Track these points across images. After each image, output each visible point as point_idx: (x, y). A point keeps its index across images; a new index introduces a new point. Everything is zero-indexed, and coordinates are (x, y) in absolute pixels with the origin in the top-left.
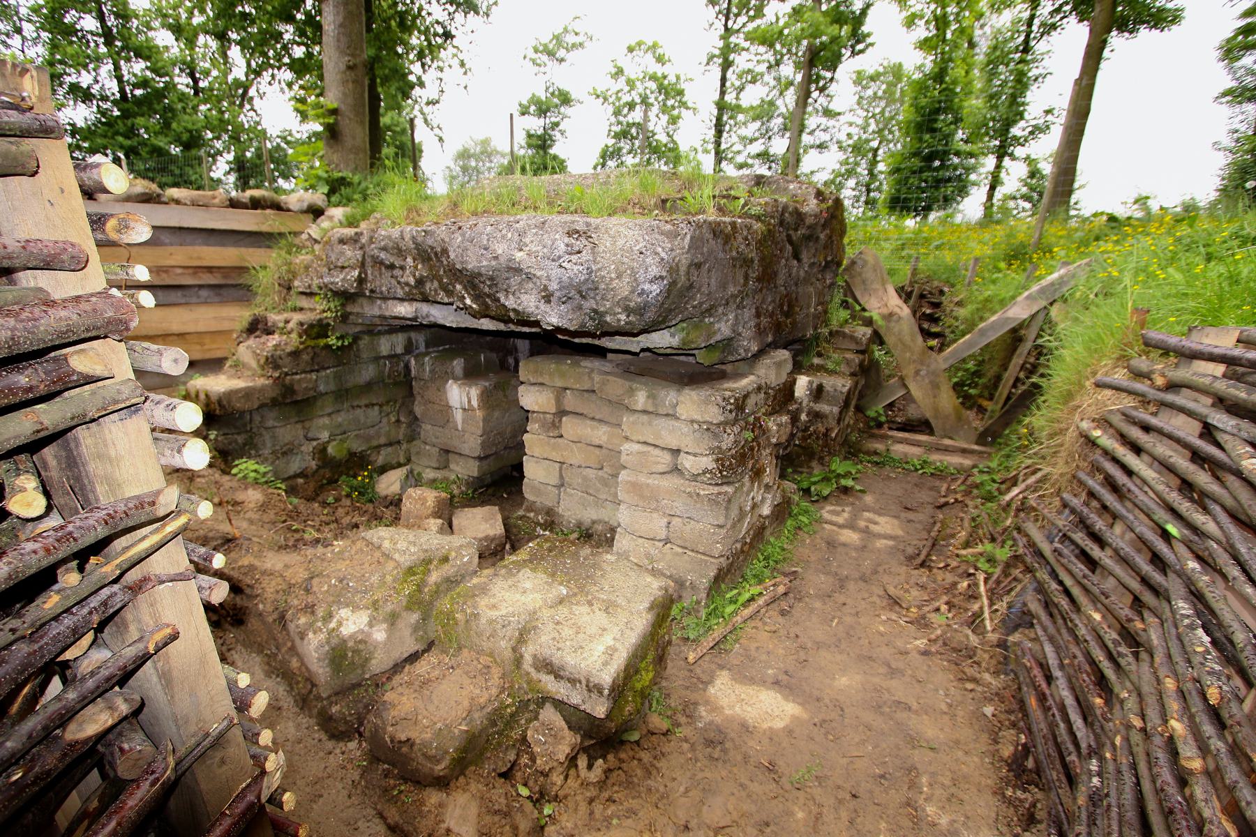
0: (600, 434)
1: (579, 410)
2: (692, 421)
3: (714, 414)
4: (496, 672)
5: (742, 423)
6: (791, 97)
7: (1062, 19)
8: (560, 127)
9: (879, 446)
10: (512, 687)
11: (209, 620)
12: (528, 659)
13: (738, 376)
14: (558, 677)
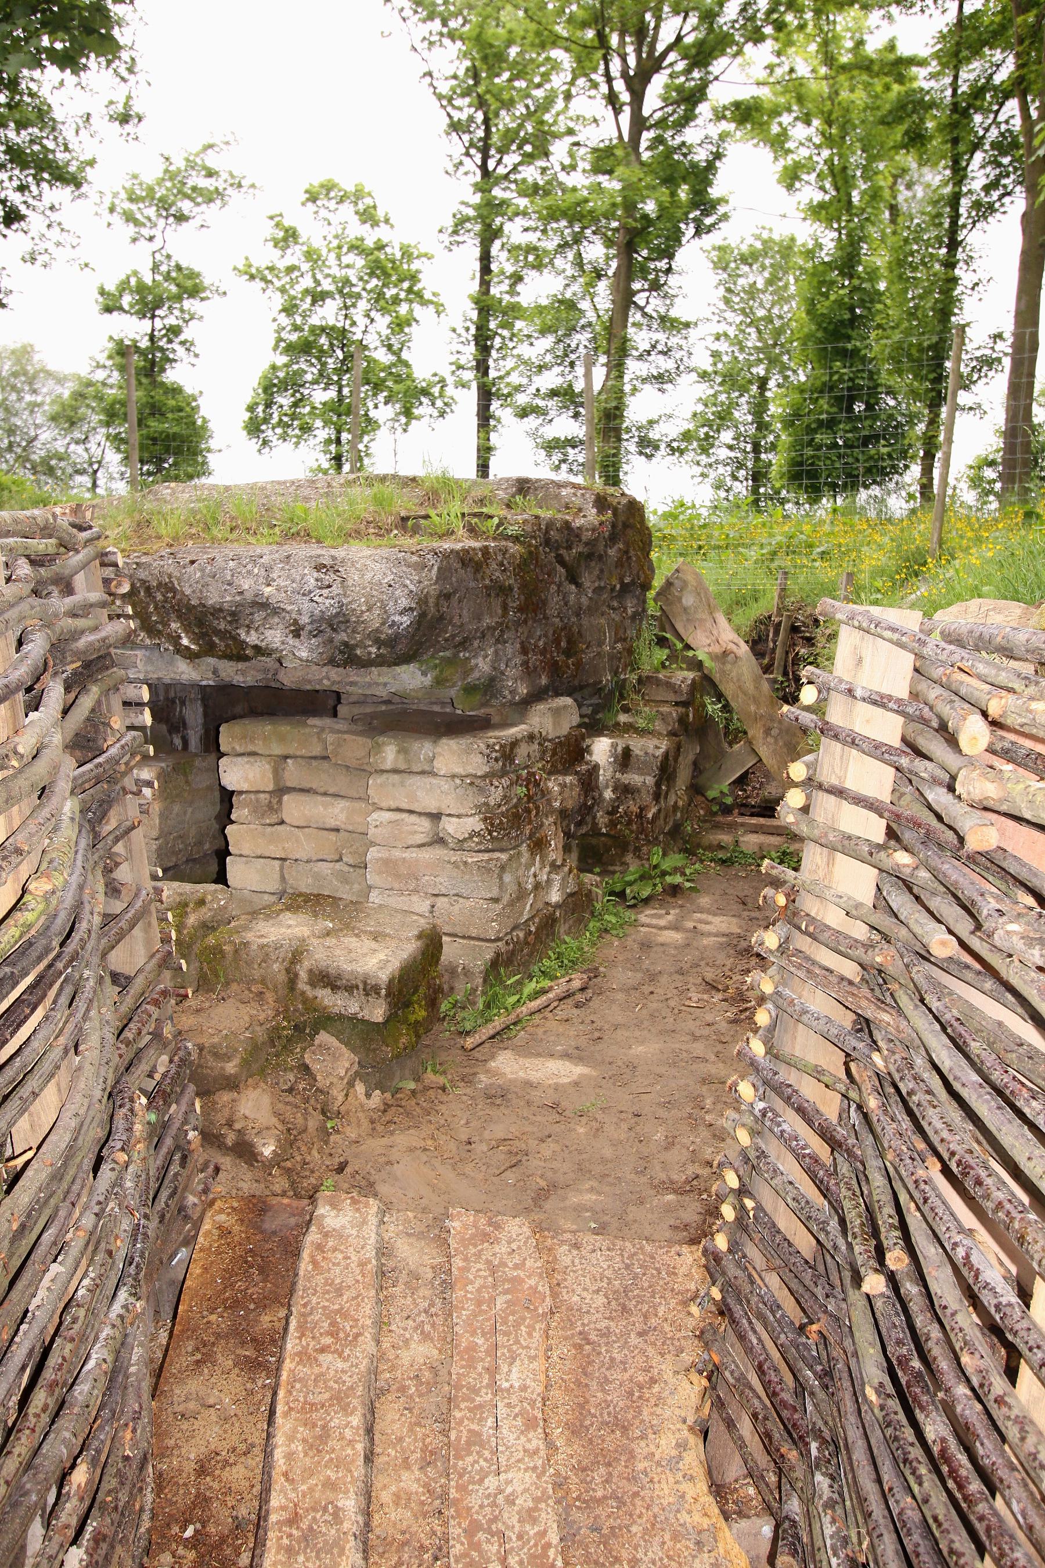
0: (337, 812)
1: (306, 785)
2: (453, 776)
3: (478, 765)
4: (270, 997)
5: (513, 776)
6: (604, 294)
7: (1003, 196)
8: (182, 337)
9: (725, 838)
10: (287, 1010)
12: (303, 975)
13: (505, 725)
14: (335, 988)
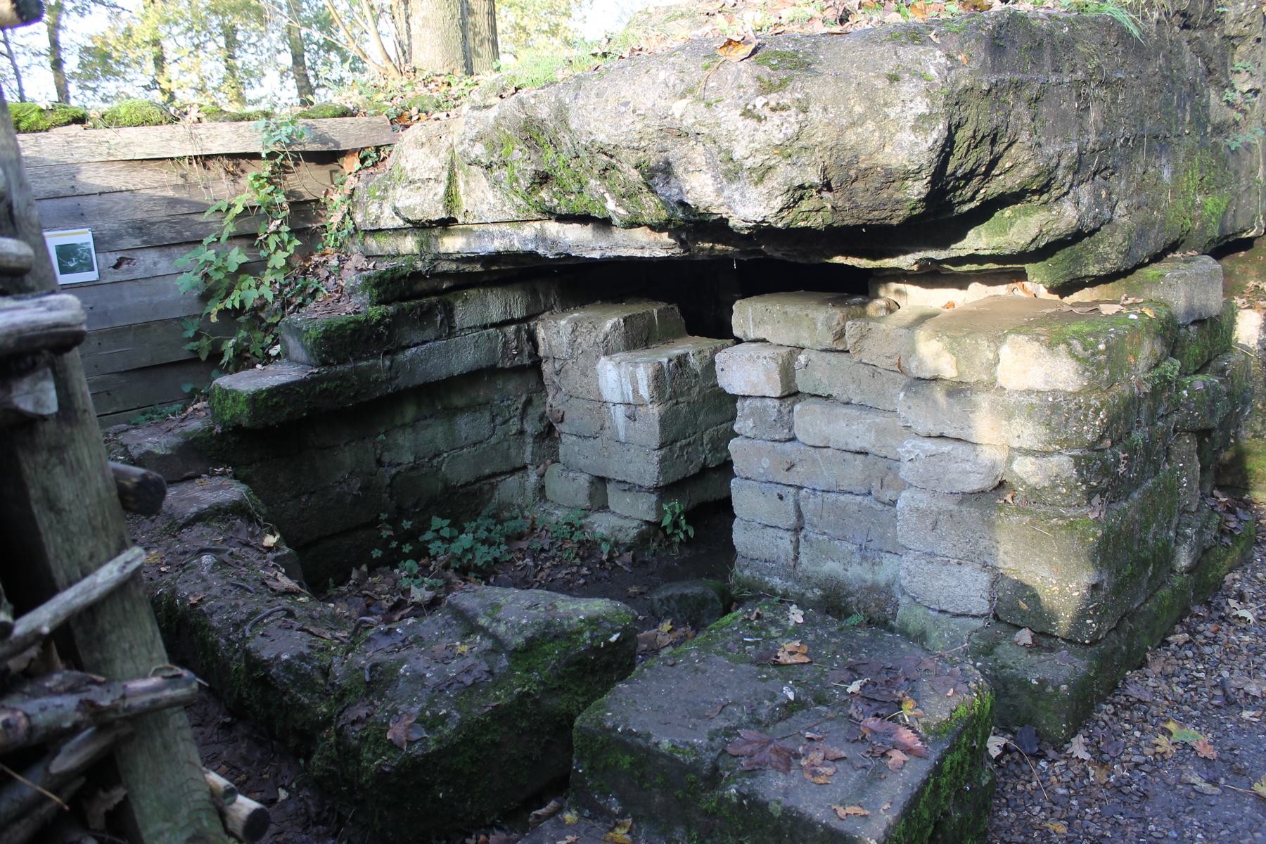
11: (261, 392)
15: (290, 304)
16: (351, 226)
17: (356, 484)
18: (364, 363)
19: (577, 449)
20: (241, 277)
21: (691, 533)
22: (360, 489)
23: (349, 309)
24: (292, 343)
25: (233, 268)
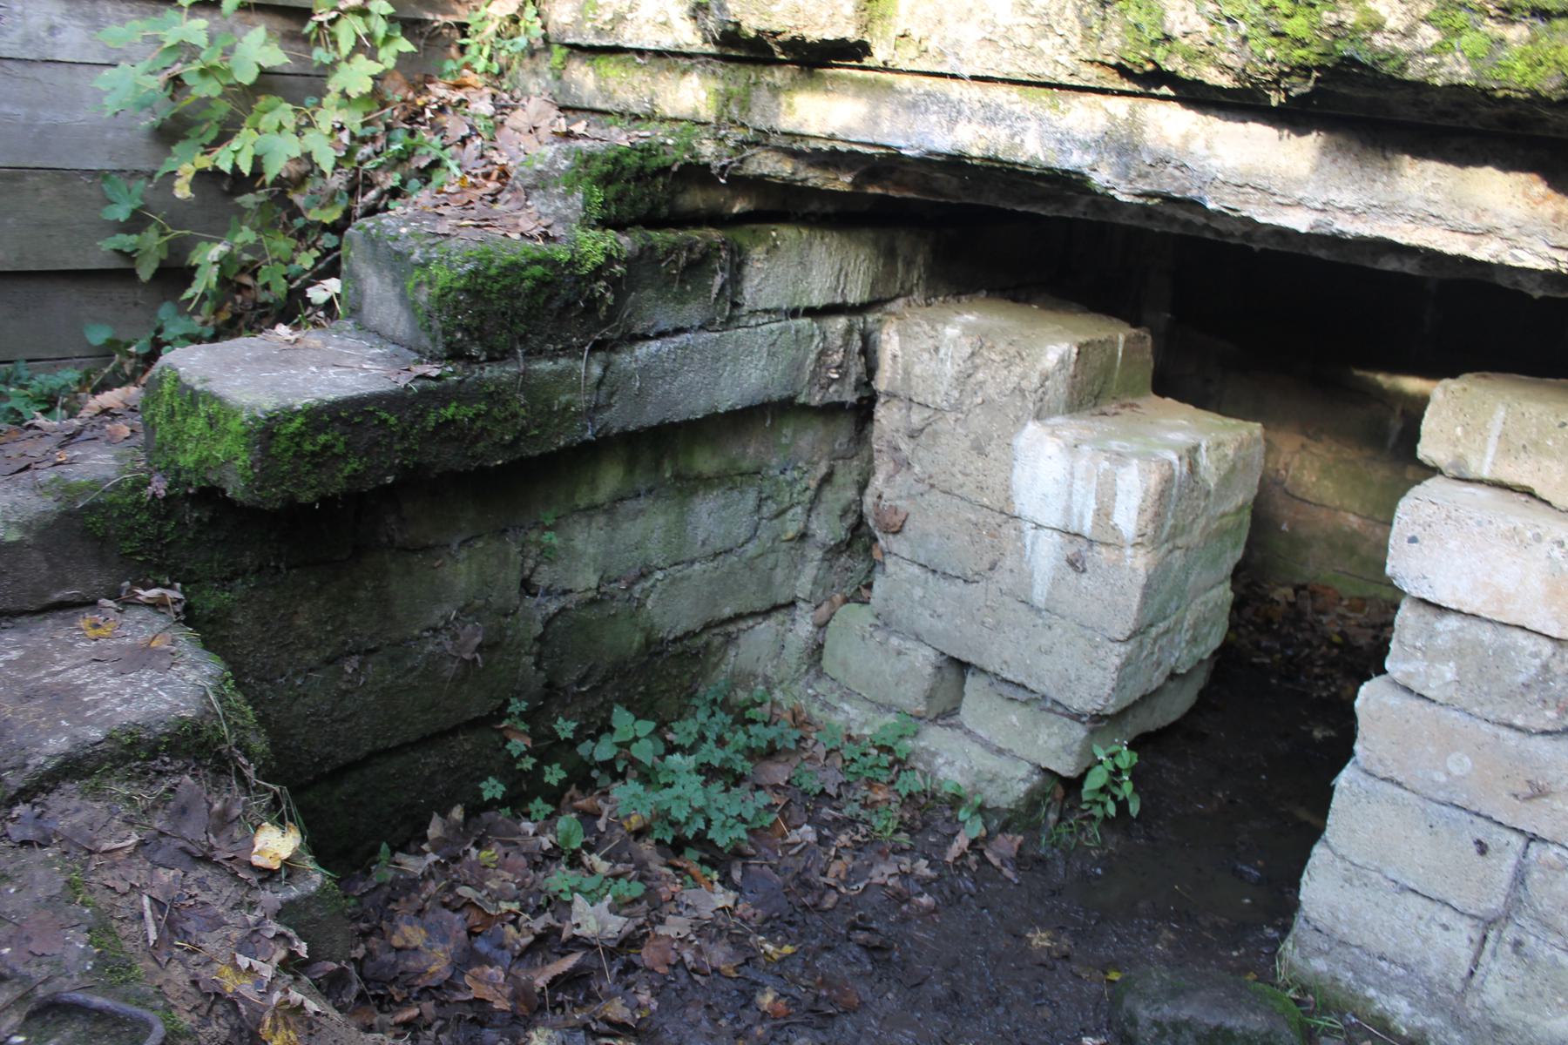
11: (290, 414)
15: (370, 185)
16: (536, 31)
17: (473, 634)
18: (545, 366)
19: (918, 592)
20: (264, 101)
21: (1134, 808)
22: (479, 648)
23: (527, 225)
24: (376, 286)
25: (248, 77)
